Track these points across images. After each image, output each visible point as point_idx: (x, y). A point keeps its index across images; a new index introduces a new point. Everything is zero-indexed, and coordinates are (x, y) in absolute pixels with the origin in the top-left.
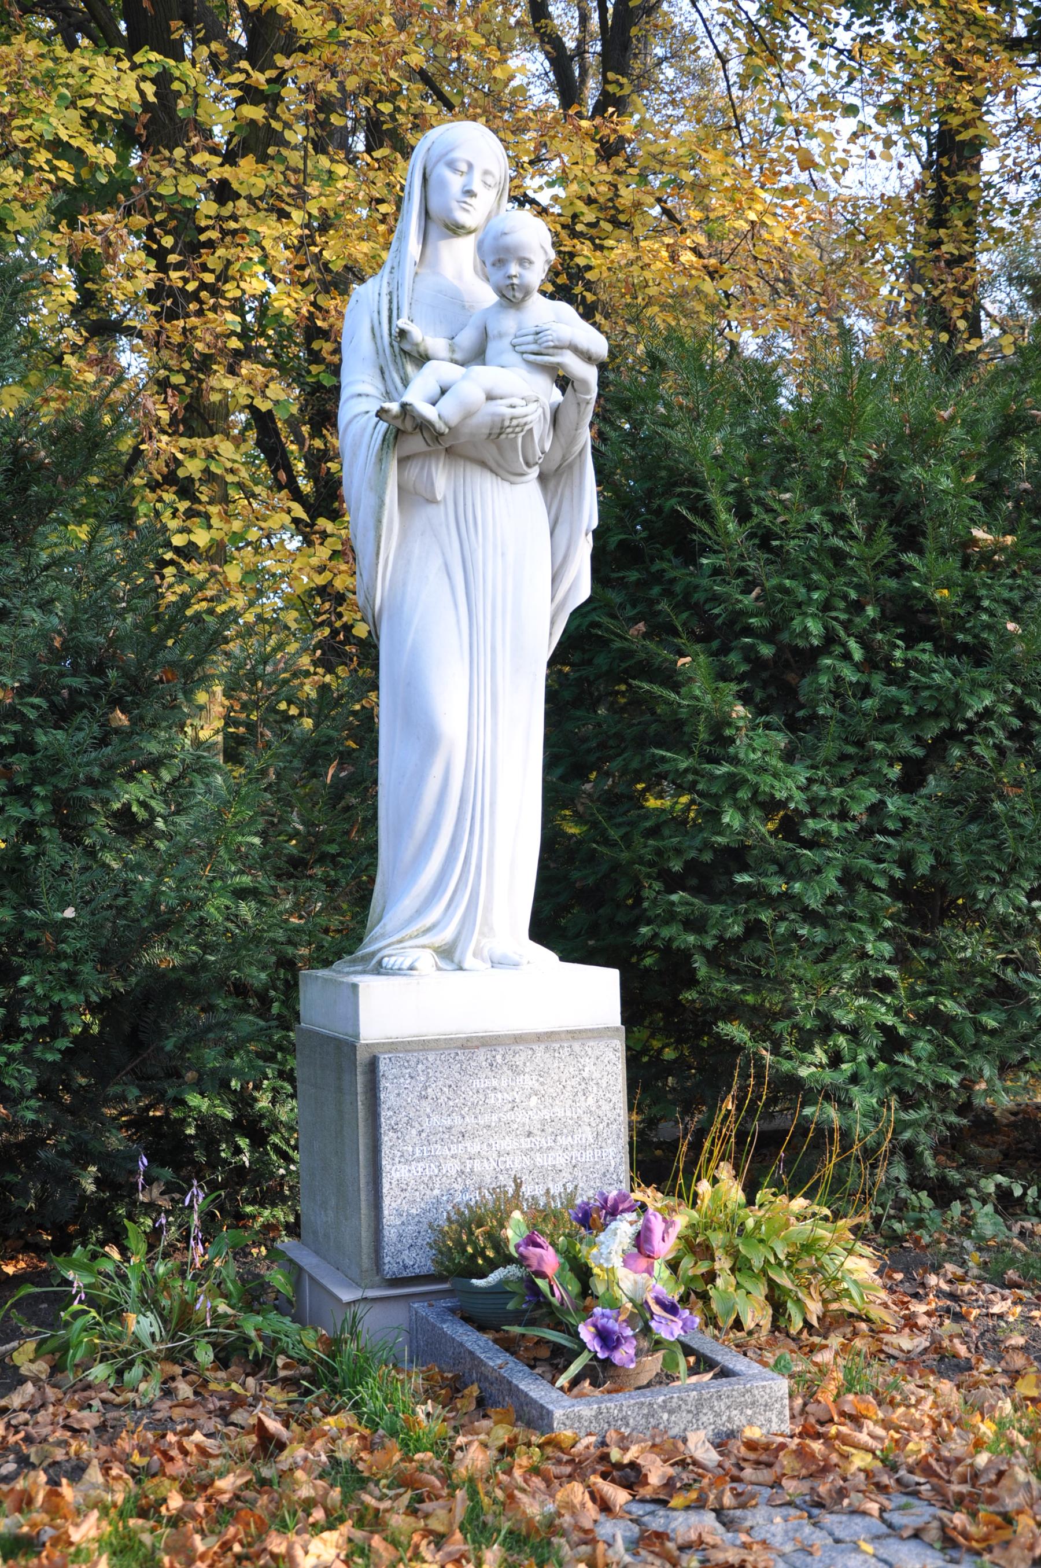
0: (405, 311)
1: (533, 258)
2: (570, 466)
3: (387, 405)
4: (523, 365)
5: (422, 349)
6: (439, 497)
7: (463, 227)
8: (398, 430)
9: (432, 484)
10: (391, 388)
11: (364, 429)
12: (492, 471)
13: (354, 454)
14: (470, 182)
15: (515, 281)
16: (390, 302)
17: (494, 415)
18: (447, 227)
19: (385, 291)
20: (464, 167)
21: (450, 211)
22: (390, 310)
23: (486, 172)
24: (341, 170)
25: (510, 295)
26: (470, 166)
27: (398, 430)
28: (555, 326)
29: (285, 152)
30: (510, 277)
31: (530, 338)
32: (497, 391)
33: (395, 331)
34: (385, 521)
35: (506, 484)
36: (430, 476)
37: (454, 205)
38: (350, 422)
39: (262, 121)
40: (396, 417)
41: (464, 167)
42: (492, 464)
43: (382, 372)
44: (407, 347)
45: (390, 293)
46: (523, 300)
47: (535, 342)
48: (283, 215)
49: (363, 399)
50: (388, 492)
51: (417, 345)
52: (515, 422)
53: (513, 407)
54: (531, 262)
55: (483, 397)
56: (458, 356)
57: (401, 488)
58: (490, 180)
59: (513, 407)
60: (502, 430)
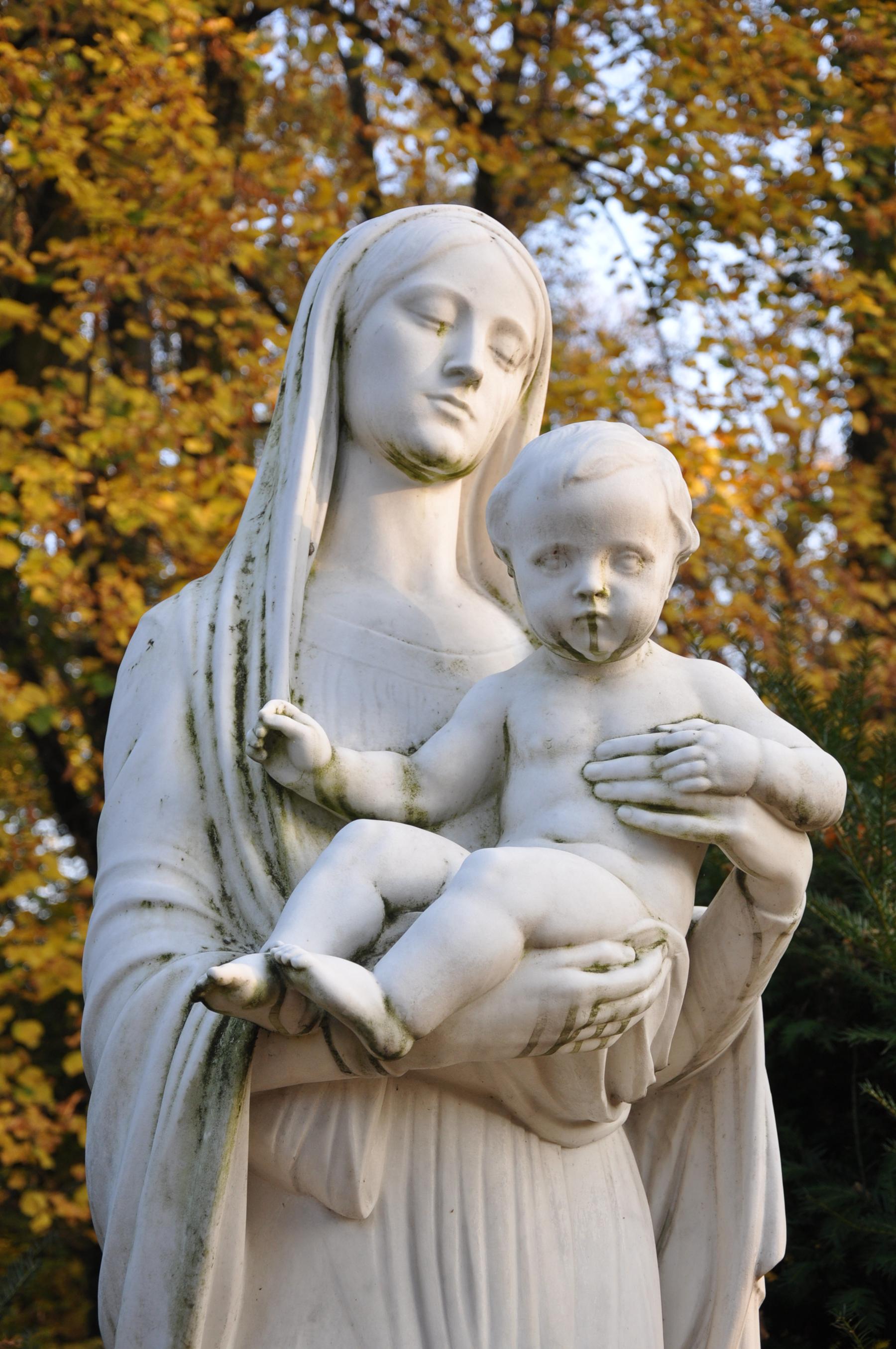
0: (282, 679)
1: (649, 545)
2: (707, 1079)
3: (227, 972)
4: (618, 837)
5: (328, 783)
6: (367, 1208)
7: (441, 461)
8: (256, 1030)
9: (350, 1174)
10: (238, 887)
11: (156, 1010)
12: (515, 1120)
13: (123, 1082)
14: (464, 347)
15: (601, 607)
16: (242, 648)
17: (547, 993)
18: (397, 459)
19: (228, 618)
20: (446, 311)
21: (408, 418)
22: (241, 670)
23: (503, 327)
24: (139, 397)
25: (580, 642)
26: (464, 309)
27: (256, 1030)
28: (713, 733)
29: (67, 375)
30: (586, 596)
31: (640, 763)
32: (560, 925)
33: (254, 733)
34: (204, 1302)
35: (551, 1152)
36: (342, 1143)
37: (421, 404)
38: (116, 982)
39: (29, 326)
40: (255, 1003)
41: (446, 311)
42: (521, 1107)
43: (213, 839)
44: (287, 777)
45: (242, 626)
46: (617, 655)
47: (656, 775)
48: (55, 453)
49: (157, 917)
50: (219, 1214)
51: (316, 772)
52: (605, 1012)
53: (600, 967)
54: (645, 558)
55: (515, 940)
56: (427, 802)
57: (254, 1173)
58: (511, 346)
59: (600, 967)
60: (568, 1032)
